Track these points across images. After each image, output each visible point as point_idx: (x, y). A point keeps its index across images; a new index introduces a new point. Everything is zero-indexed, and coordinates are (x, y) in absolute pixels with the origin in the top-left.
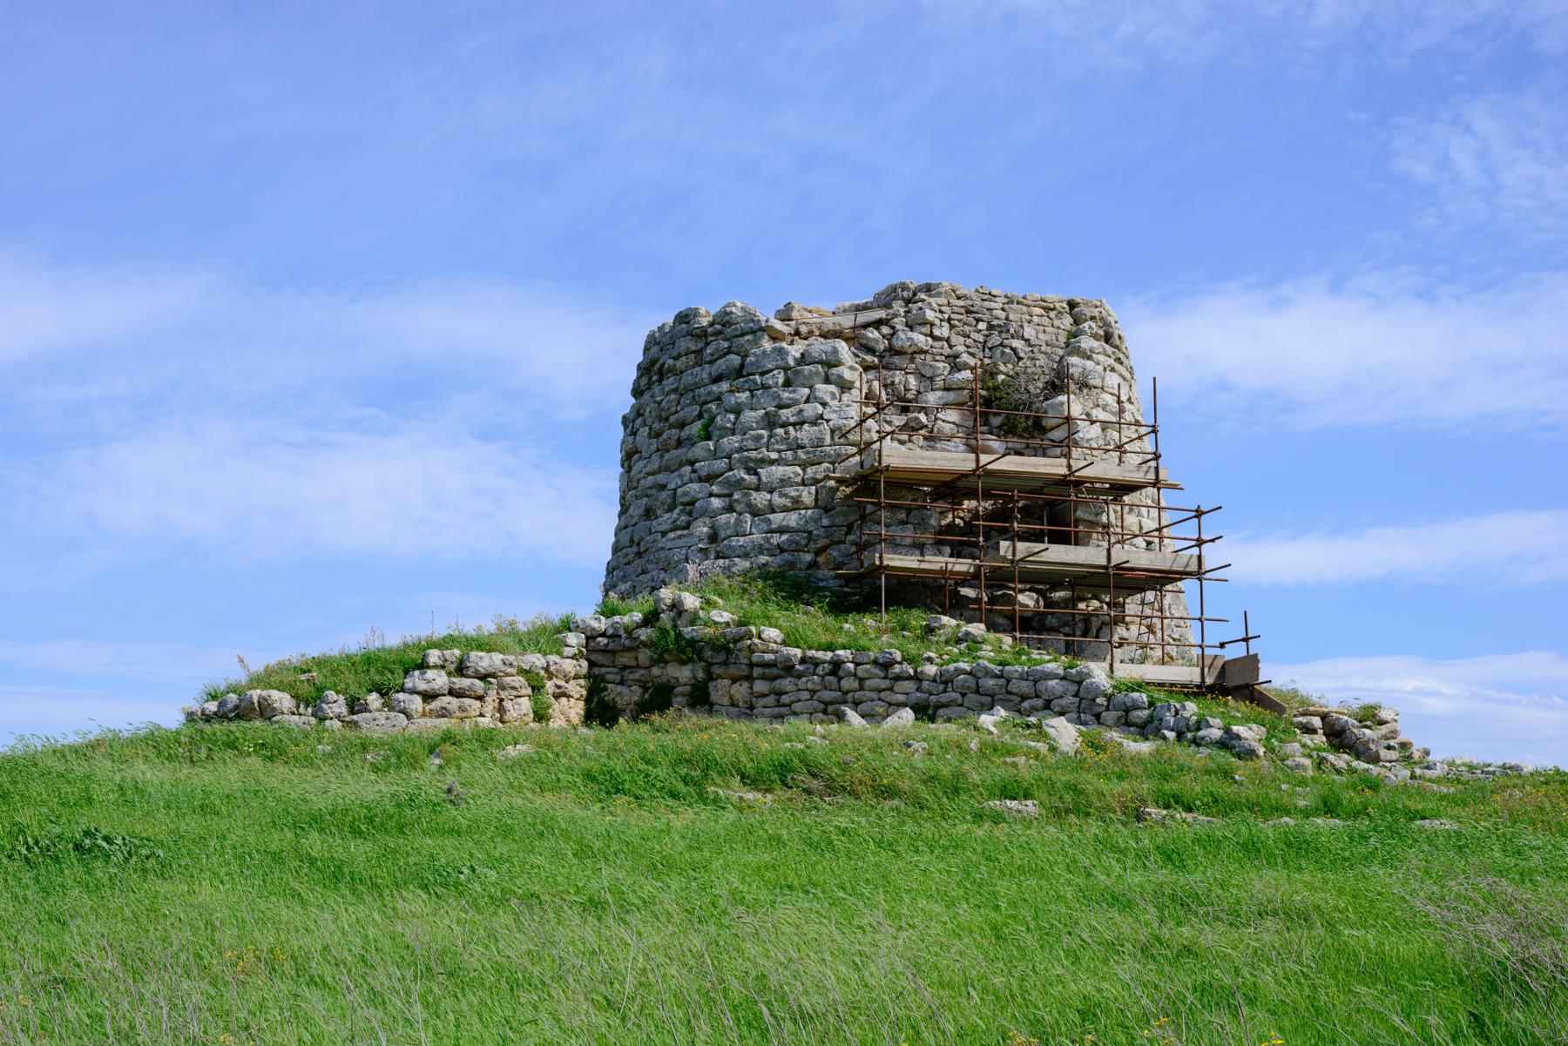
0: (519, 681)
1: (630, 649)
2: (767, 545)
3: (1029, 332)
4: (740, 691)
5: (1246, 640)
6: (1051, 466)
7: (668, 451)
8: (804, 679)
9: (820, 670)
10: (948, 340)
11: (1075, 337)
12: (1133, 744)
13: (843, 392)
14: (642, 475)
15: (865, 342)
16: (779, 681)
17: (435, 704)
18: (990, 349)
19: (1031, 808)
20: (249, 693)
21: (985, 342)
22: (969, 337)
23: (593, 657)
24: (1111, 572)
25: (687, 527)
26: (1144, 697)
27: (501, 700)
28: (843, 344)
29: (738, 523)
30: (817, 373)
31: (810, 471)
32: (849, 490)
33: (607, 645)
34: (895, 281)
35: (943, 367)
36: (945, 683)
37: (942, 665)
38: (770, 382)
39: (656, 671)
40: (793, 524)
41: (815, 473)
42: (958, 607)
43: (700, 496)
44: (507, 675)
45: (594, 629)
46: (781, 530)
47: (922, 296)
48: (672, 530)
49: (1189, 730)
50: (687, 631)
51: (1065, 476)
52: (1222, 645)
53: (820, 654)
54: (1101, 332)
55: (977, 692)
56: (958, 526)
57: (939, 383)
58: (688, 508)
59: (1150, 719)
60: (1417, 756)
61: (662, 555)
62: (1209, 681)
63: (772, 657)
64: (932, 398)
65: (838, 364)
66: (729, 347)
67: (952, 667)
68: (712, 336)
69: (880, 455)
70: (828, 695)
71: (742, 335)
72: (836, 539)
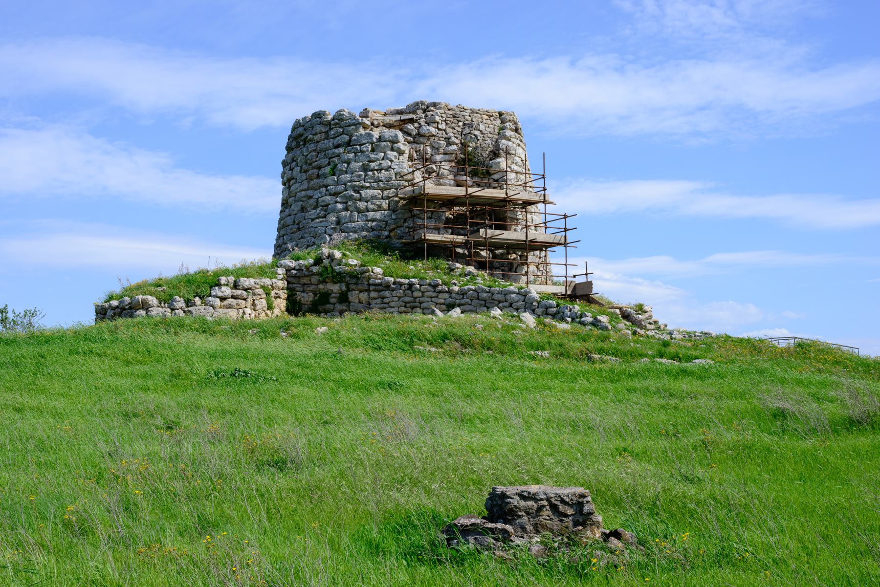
0: (260, 291)
1: (307, 276)
2: (366, 227)
3: (482, 127)
4: (364, 296)
5: (586, 274)
6: (498, 193)
7: (312, 180)
8: (395, 292)
9: (403, 287)
10: (445, 130)
11: (503, 130)
12: (554, 323)
13: (400, 155)
14: (298, 190)
15: (406, 130)
16: (383, 292)
17: (226, 302)
18: (464, 135)
19: (546, 354)
20: (137, 297)
21: (462, 131)
22: (454, 129)
23: (289, 280)
24: (528, 243)
25: (325, 217)
26: (554, 302)
27: (254, 300)
28: (400, 132)
29: (351, 216)
30: (388, 146)
31: (386, 193)
32: (404, 202)
33: (296, 274)
34: (418, 100)
35: (443, 143)
36: (463, 295)
37: (461, 287)
38: (365, 149)
39: (321, 286)
40: (378, 217)
41: (389, 193)
42: (458, 257)
43: (331, 202)
44: (256, 288)
45: (289, 266)
46: (373, 220)
47: (432, 108)
48: (317, 218)
49: (577, 318)
50: (337, 268)
51: (505, 198)
52: (574, 276)
53: (403, 280)
54: (514, 128)
55: (478, 299)
56: (450, 218)
57: (441, 151)
58: (325, 208)
59: (558, 313)
60: (662, 327)
61: (313, 230)
62: (569, 292)
63: (380, 281)
64: (438, 158)
65: (398, 142)
66: (343, 131)
67: (466, 287)
68: (333, 125)
69: (424, 188)
70: (407, 299)
71: (350, 126)
72: (399, 225)
